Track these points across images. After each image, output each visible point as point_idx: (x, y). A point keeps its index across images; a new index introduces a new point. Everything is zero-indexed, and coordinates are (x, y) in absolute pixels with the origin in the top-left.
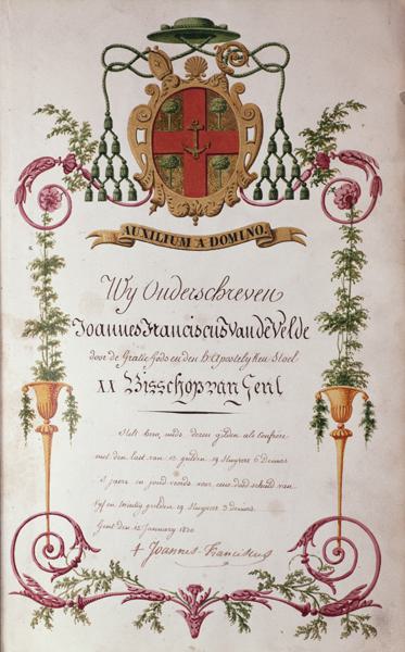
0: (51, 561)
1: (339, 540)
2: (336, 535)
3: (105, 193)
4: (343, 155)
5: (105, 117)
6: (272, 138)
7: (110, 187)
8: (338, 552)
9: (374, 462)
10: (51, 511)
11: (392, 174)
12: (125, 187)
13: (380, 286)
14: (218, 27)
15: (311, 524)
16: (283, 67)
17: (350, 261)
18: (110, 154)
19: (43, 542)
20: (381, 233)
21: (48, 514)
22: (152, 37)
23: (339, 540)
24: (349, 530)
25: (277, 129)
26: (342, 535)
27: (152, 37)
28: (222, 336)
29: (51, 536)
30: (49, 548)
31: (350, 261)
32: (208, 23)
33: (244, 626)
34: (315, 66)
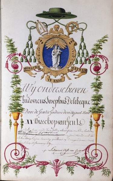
0: (17, 156)
1: (96, 150)
2: (95, 149)
3: (27, 59)
4: (66, 163)
5: (6, 62)
6: (79, 52)
7: (28, 58)
8: (96, 154)
9: (104, 136)
10: (17, 142)
11: (110, 63)
12: (33, 58)
13: (106, 91)
14: (66, 13)
15: (89, 144)
16: (84, 30)
17: (98, 86)
18: (29, 47)
19: (14, 152)
20: (106, 78)
21: (16, 143)
22: (39, 15)
23: (96, 150)
24: (98, 147)
25: (80, 49)
26: (97, 149)
27: (39, 15)
28: (65, 103)
29: (17, 151)
30: (16, 154)
31: (98, 86)
32: (62, 10)
33: (72, 173)
34: (92, 29)
